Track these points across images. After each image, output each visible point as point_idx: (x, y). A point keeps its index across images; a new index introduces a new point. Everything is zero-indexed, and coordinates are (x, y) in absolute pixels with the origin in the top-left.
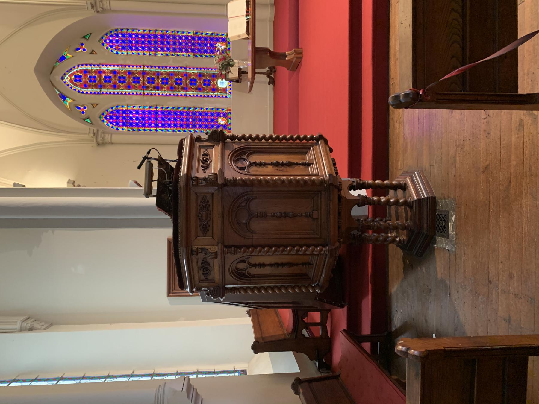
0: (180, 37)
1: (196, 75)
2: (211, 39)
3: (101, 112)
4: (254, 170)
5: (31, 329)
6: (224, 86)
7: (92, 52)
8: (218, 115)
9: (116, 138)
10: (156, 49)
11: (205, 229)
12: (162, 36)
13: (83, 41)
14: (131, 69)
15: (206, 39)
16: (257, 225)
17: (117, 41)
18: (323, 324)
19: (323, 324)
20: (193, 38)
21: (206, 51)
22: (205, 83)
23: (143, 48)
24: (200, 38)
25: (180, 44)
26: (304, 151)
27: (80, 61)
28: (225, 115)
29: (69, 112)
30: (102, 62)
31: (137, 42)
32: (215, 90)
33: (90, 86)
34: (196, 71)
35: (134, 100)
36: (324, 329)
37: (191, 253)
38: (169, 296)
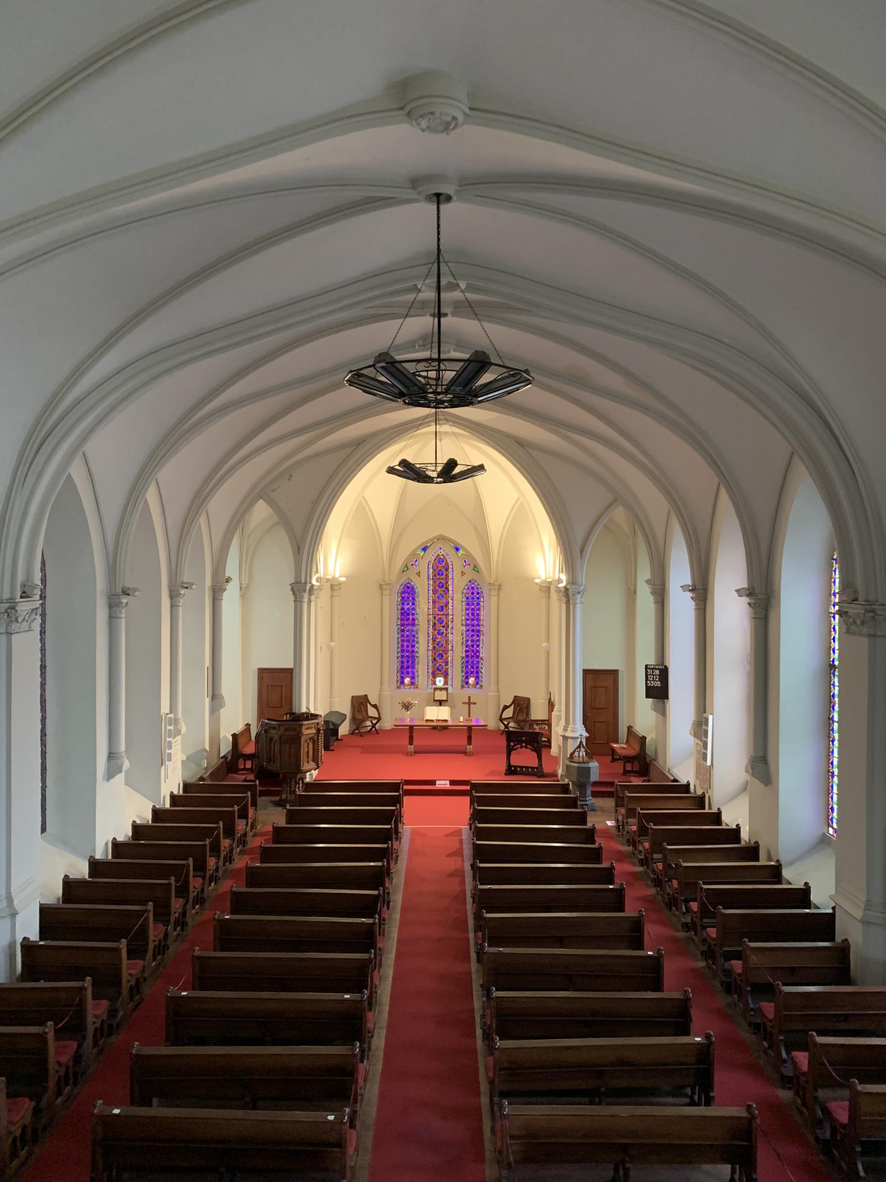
0: (478, 646)
1: (447, 658)
2: (477, 672)
3: (413, 579)
4: (306, 745)
5: (241, 589)
6: (437, 683)
7: (463, 573)
8: (413, 678)
9: (386, 599)
10: (467, 625)
11: (286, 730)
12: (479, 631)
13: (472, 566)
14: (450, 604)
15: (477, 667)
16: (287, 745)
17: (473, 593)
18: (245, 769)
19: (245, 769)
20: (478, 657)
21: (467, 667)
22: (439, 668)
23: (468, 614)
24: (478, 662)
25: (473, 646)
26: (313, 761)
27: (455, 561)
28: (412, 683)
29: (414, 554)
30: (455, 581)
31: (473, 609)
32: (434, 676)
33: (434, 570)
34: (450, 659)
35: (423, 607)
36: (242, 770)
37: (279, 726)
38: (259, 669)
